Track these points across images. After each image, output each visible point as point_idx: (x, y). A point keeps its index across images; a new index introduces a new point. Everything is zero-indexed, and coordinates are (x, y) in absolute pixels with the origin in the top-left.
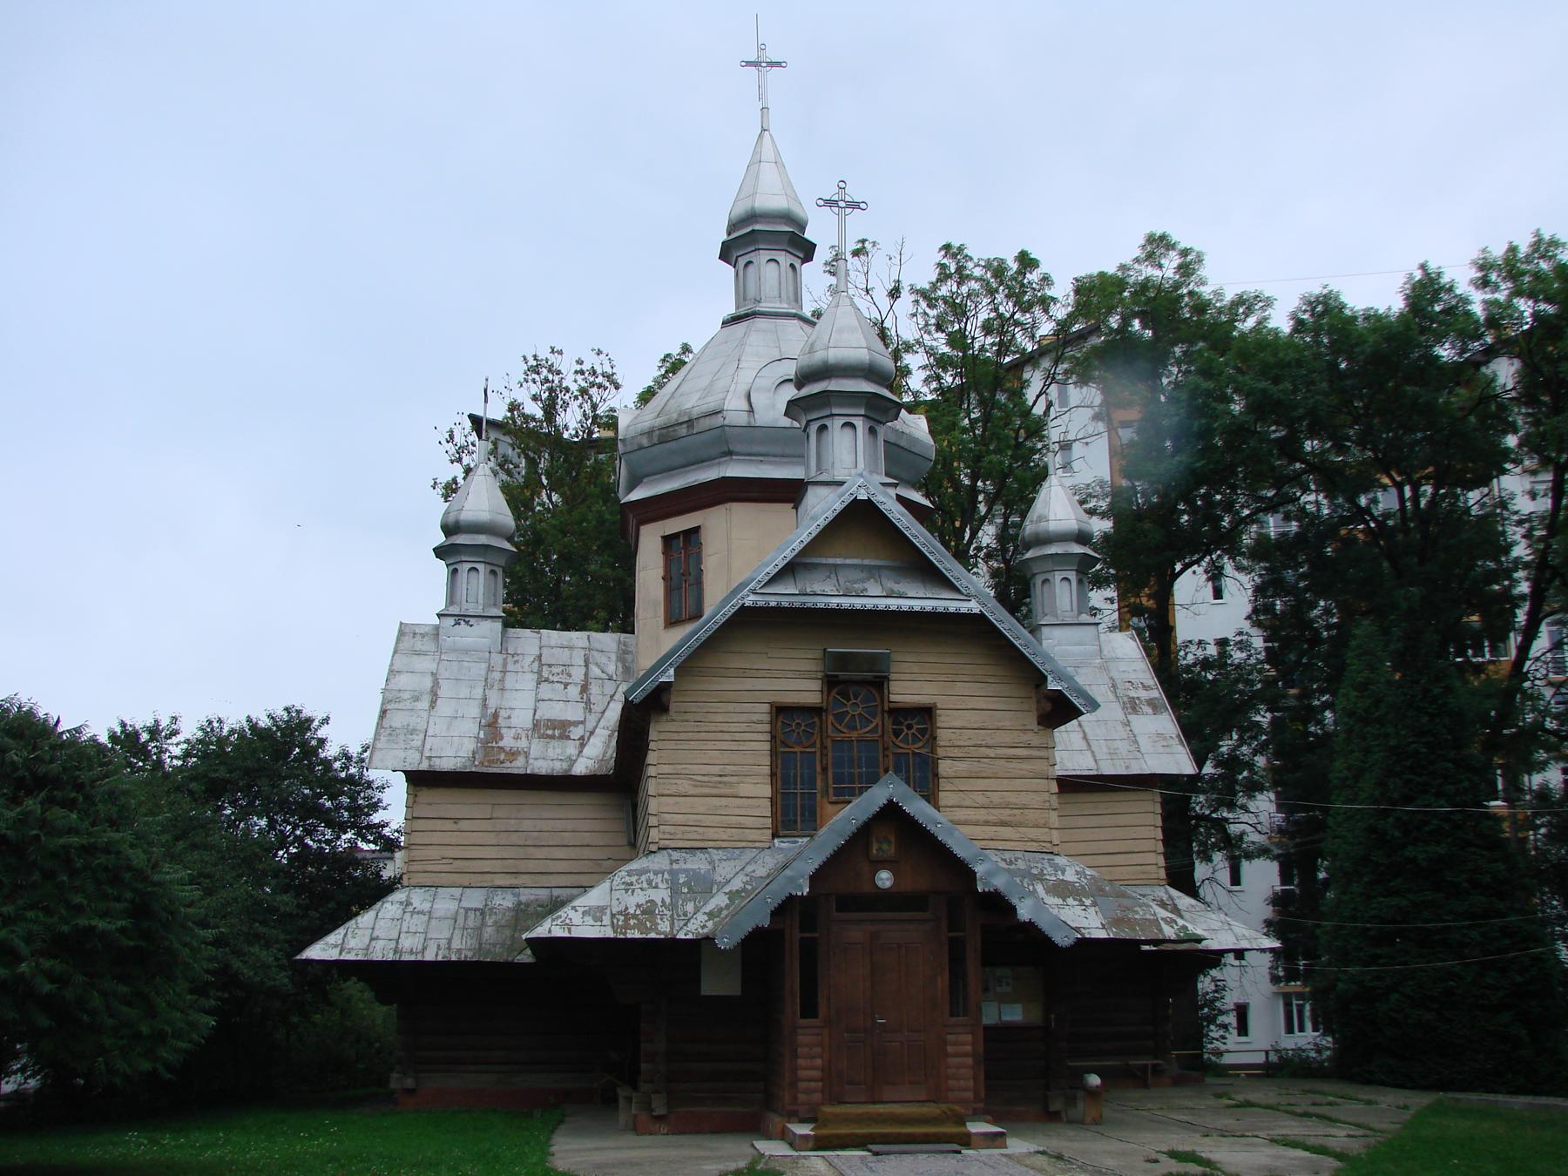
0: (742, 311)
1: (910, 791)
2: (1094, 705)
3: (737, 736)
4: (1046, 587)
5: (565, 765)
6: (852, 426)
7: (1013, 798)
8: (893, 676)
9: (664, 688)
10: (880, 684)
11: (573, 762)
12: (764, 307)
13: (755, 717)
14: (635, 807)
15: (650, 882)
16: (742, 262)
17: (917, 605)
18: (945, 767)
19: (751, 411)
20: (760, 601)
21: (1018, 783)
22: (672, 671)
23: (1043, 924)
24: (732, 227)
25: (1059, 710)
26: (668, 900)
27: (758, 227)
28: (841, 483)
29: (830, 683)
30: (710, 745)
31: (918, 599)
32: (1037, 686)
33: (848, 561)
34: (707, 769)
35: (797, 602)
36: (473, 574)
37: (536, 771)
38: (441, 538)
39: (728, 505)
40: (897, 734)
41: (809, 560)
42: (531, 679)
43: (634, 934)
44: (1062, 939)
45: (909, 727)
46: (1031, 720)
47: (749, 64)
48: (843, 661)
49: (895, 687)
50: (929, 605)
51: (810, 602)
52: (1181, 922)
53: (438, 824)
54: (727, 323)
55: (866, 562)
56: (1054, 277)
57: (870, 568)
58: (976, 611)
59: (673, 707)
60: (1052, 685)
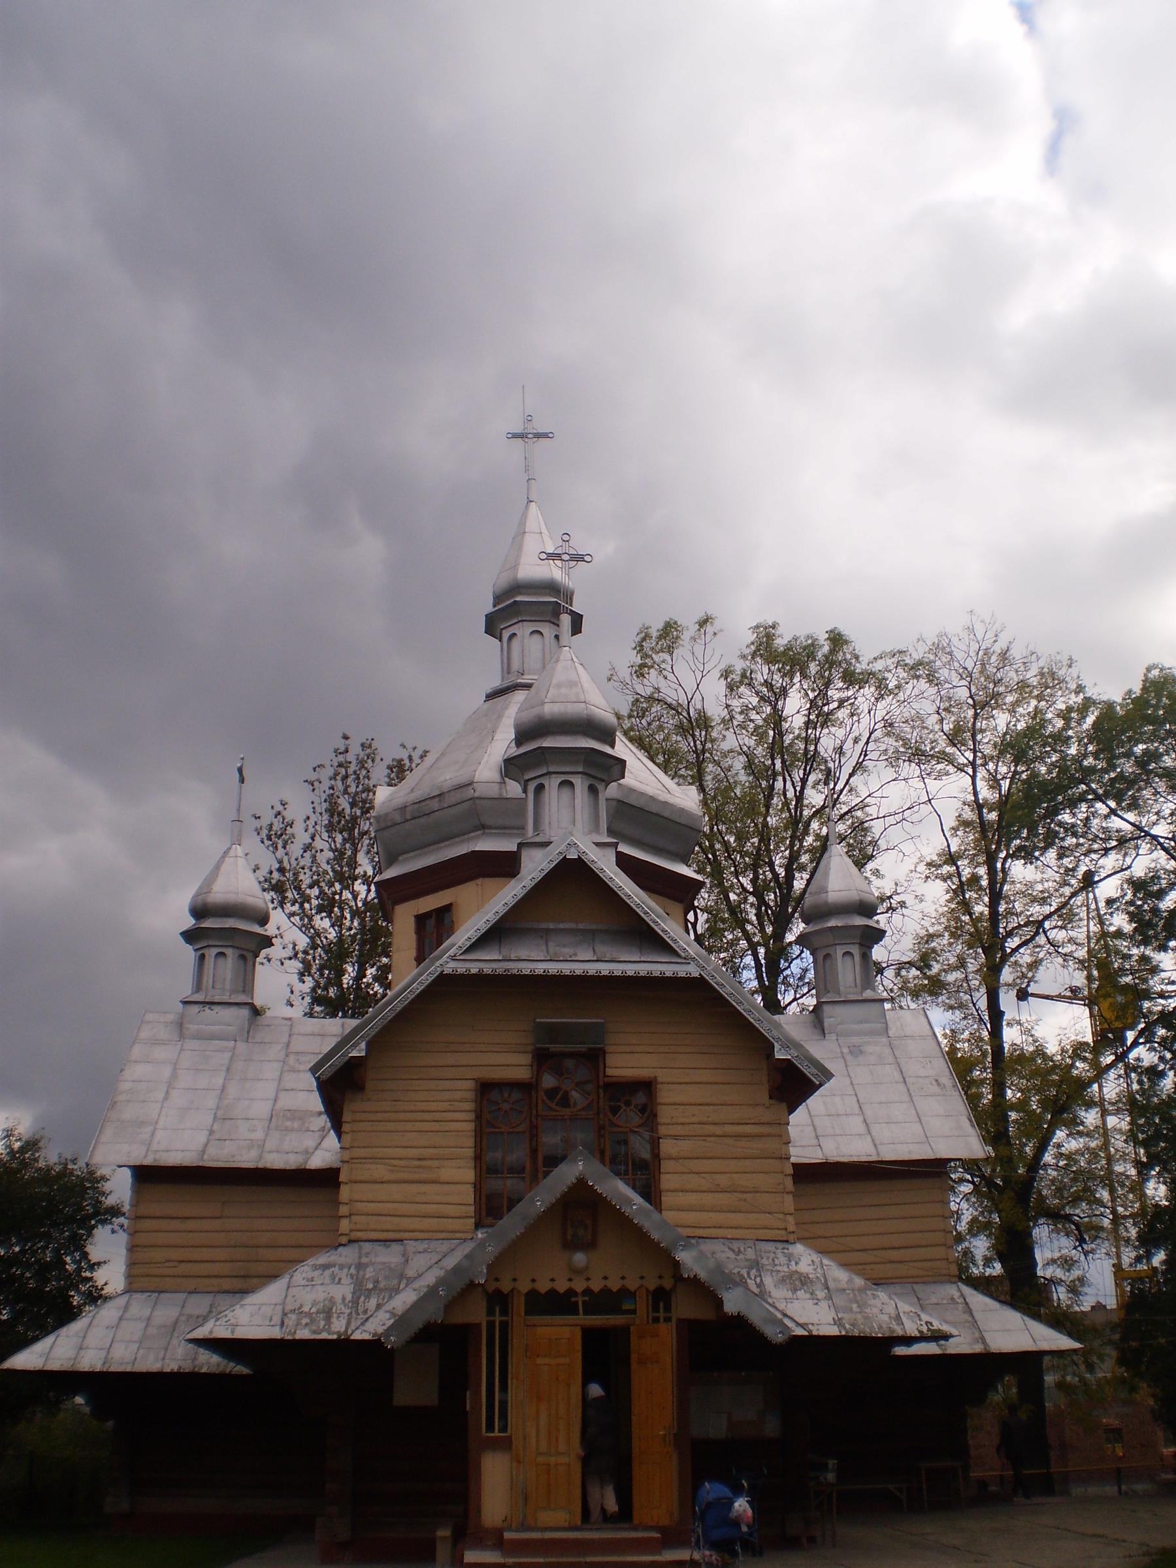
0: (506, 684)
1: (606, 1170)
2: (828, 1075)
3: (438, 1116)
4: (828, 962)
5: (254, 1153)
6: (571, 784)
8: (609, 1049)
9: (354, 1065)
10: (595, 1057)
11: (308, 1153)
13: (458, 1095)
15: (333, 1276)
16: (506, 635)
17: (631, 970)
20: (461, 968)
22: (363, 1045)
23: (755, 1317)
24: (498, 599)
26: (349, 1297)
29: (542, 1059)
30: (409, 1126)
33: (561, 926)
34: (402, 1152)
35: (500, 968)
36: (221, 960)
37: (269, 1166)
38: (190, 922)
39: (479, 881)
40: (615, 1110)
43: (304, 1334)
44: (775, 1336)
46: (763, 1095)
47: (515, 436)
48: (552, 1032)
49: (611, 1060)
50: (643, 969)
51: (514, 968)
52: (925, 1317)
53: (163, 1224)
54: (491, 696)
55: (581, 926)
57: (584, 932)
59: (369, 1085)
60: (780, 1055)
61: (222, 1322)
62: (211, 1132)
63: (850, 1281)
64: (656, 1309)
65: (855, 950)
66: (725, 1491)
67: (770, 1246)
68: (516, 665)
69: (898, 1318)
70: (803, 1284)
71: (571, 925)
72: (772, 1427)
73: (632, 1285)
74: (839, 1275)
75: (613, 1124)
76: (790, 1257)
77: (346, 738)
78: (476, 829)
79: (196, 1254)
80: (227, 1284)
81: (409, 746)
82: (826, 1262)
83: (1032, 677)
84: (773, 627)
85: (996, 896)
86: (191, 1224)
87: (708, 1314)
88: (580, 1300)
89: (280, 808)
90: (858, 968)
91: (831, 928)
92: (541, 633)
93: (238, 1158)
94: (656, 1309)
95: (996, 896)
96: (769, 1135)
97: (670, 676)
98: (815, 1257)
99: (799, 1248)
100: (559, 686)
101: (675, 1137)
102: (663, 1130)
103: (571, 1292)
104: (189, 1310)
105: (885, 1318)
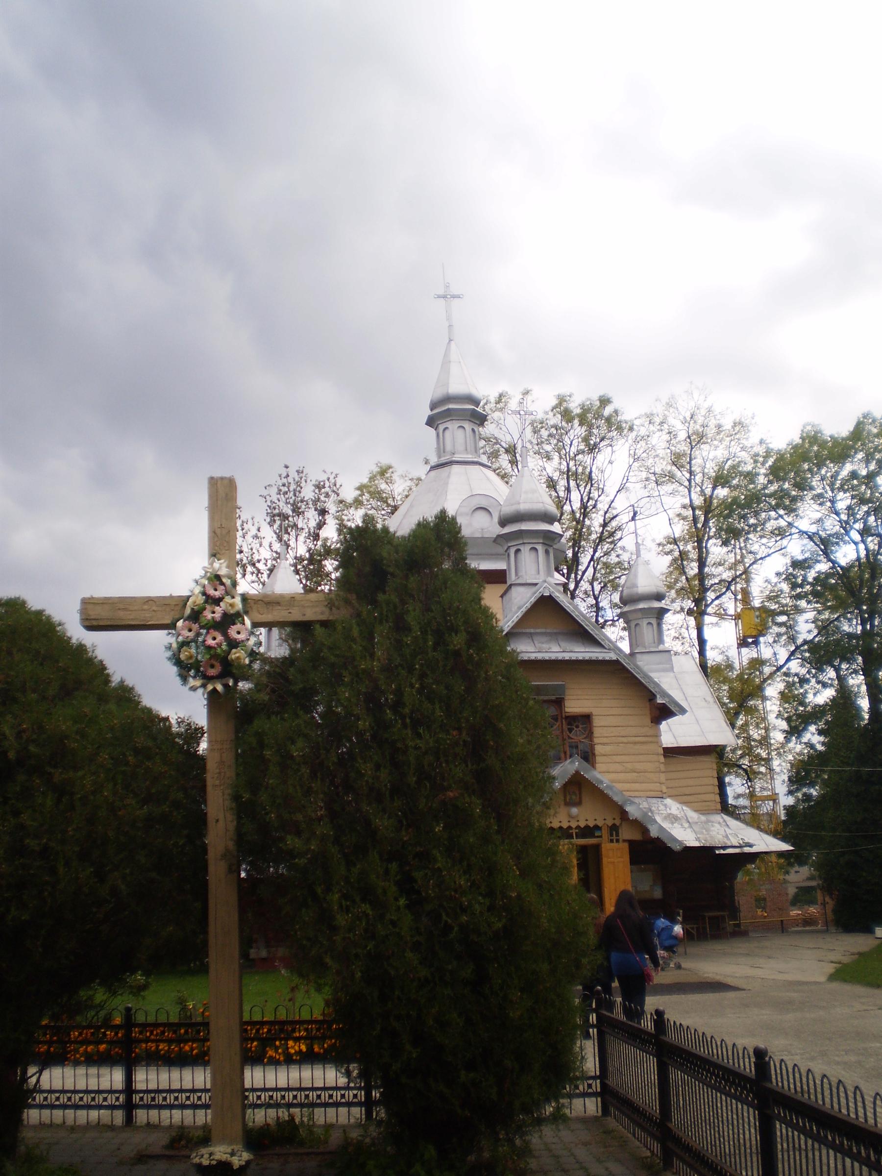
0: (443, 460)
4: (637, 628)
6: (536, 549)
7: (638, 766)
10: (559, 702)
12: (457, 458)
16: (441, 427)
17: (580, 656)
18: (598, 749)
21: (642, 758)
23: (662, 837)
25: (664, 712)
27: (451, 406)
28: (536, 584)
31: (580, 652)
32: (650, 700)
33: (538, 631)
40: (570, 730)
41: (520, 631)
44: (677, 848)
45: (577, 727)
46: (648, 720)
47: (439, 297)
50: (587, 656)
55: (548, 631)
56: (610, 394)
58: (615, 658)
63: (699, 818)
64: (612, 835)
65: (654, 621)
66: (668, 923)
67: (654, 800)
68: (449, 447)
69: (727, 836)
70: (676, 820)
71: (543, 630)
72: (658, 894)
73: (600, 823)
74: (693, 815)
75: (570, 738)
76: (665, 806)
77: (287, 467)
81: (329, 471)
82: (684, 808)
83: (727, 425)
84: (570, 396)
85: (702, 563)
87: (637, 836)
88: (574, 831)
91: (641, 609)
92: (463, 428)
94: (612, 835)
95: (702, 563)
96: (651, 742)
97: (504, 428)
98: (678, 805)
99: (668, 801)
101: (604, 744)
102: (596, 740)
103: (570, 828)
105: (721, 837)
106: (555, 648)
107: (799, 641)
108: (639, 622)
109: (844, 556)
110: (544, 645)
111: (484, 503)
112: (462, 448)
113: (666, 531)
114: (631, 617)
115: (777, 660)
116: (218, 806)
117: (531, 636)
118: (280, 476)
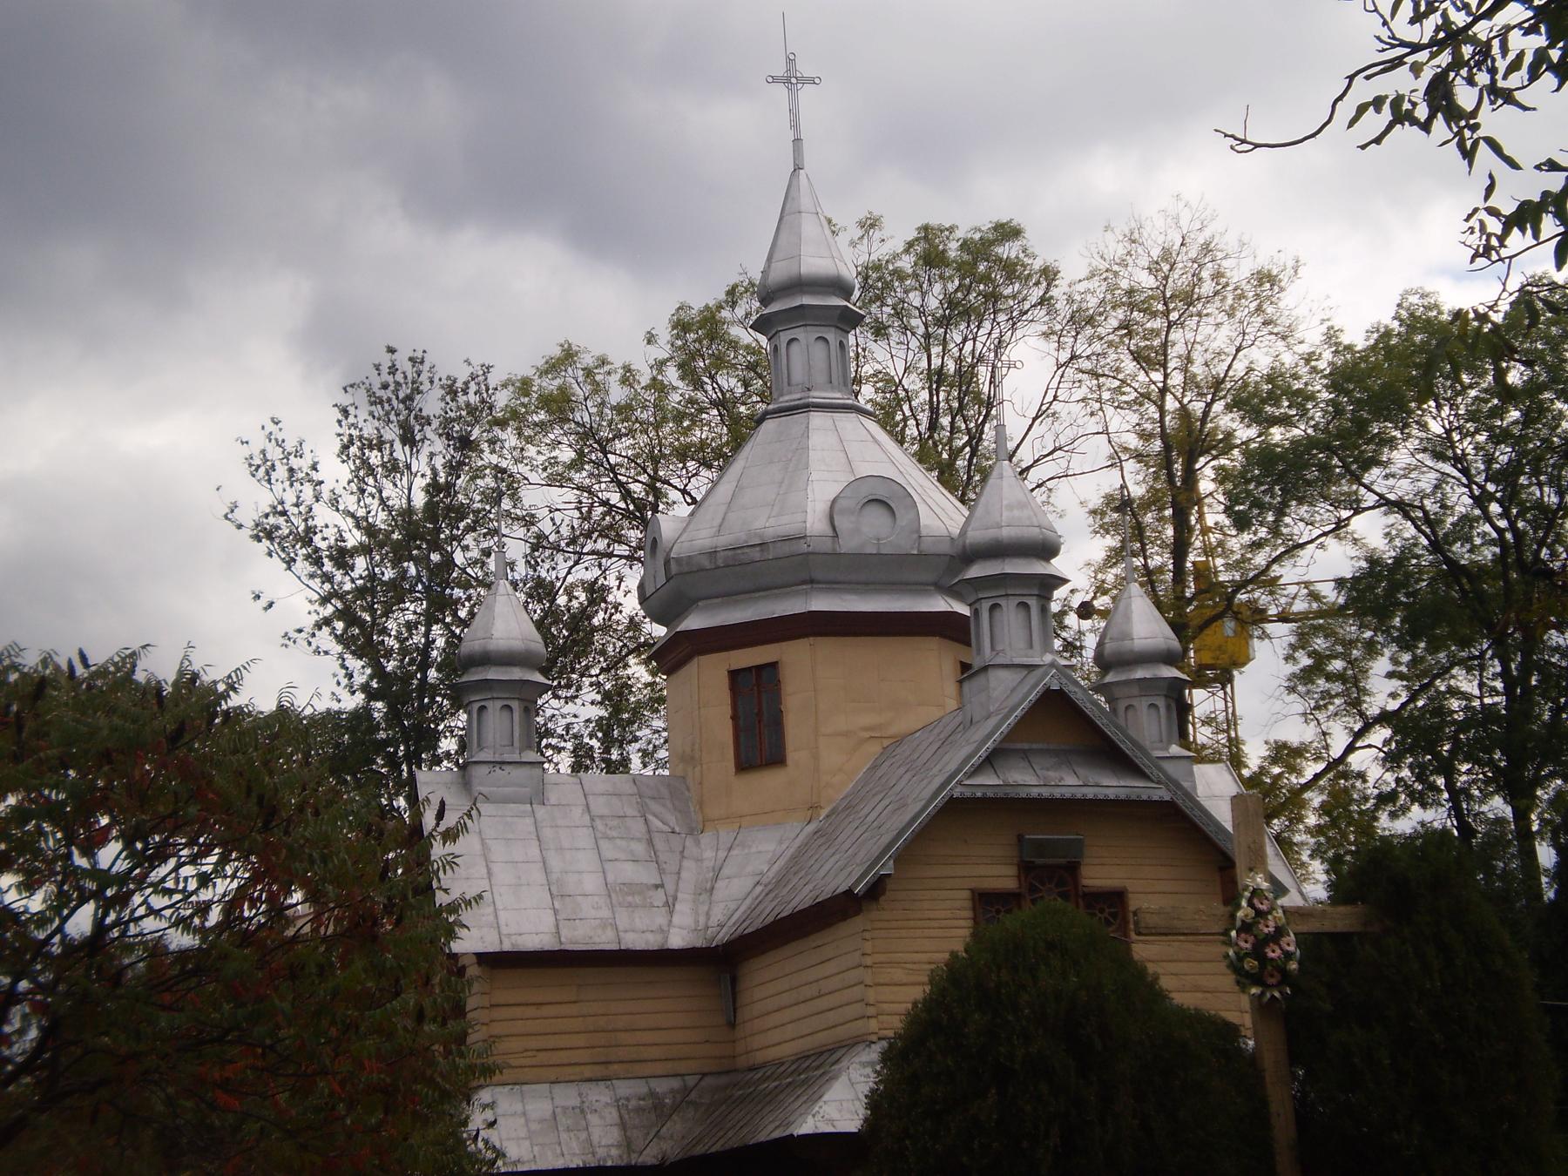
3: (945, 923)
4: (1130, 713)
6: (1025, 606)
10: (1073, 869)
12: (818, 396)
14: (734, 981)
16: (784, 337)
19: (836, 535)
27: (807, 300)
29: (1025, 868)
31: (1111, 785)
33: (1035, 746)
37: (631, 946)
42: (584, 837)
47: (775, 79)
53: (518, 1011)
55: (1052, 747)
58: (1167, 798)
61: (818, 1117)
62: (556, 912)
78: (804, 582)
79: (552, 1042)
80: (588, 1072)
81: (476, 362)
86: (546, 1011)
89: (271, 427)
90: (1163, 720)
93: (597, 940)
100: (1010, 507)
104: (559, 1101)
106: (1070, 780)
107: (1373, 711)
108: (1134, 702)
109: (1107, 228)
110: (1051, 774)
111: (881, 493)
112: (820, 378)
113: (1109, 482)
114: (1117, 693)
115: (1327, 747)
116: (1280, 1100)
117: (1025, 755)
118: (377, 367)
